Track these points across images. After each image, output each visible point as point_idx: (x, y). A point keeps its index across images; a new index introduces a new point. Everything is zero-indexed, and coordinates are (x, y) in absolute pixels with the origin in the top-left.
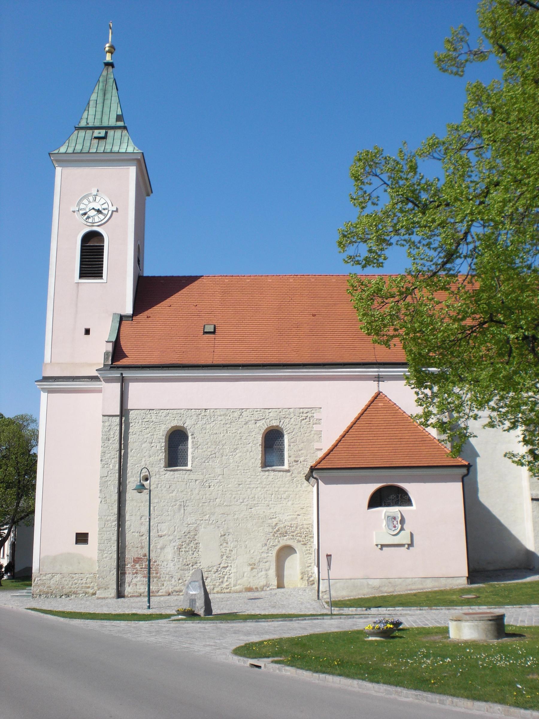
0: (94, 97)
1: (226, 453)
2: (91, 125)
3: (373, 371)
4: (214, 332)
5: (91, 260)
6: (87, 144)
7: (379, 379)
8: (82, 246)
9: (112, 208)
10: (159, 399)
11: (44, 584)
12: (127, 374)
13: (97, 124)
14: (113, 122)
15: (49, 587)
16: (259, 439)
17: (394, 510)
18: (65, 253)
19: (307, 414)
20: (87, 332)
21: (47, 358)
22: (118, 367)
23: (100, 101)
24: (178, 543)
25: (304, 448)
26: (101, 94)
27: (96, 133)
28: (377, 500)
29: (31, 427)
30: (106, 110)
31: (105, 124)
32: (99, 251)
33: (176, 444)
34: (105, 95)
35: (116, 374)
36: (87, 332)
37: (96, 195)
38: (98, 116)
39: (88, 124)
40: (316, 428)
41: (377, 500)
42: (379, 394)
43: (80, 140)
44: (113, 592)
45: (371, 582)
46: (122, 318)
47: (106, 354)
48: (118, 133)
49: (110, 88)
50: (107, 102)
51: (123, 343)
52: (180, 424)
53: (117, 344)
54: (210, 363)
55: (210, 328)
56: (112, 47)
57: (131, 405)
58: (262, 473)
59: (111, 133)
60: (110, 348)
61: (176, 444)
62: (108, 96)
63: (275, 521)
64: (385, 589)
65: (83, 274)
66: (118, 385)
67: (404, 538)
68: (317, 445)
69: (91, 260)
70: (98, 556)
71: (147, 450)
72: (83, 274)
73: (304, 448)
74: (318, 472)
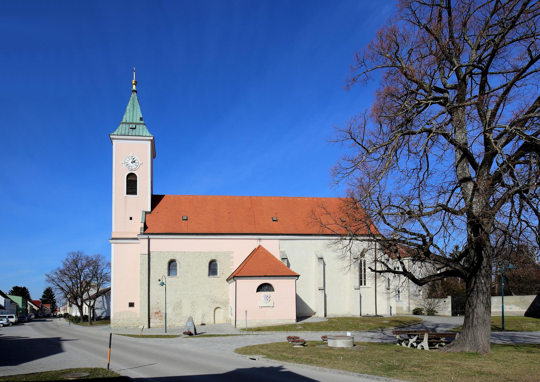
0: (128, 107)
1: (193, 269)
2: (128, 122)
4: (187, 220)
6: (127, 131)
8: (127, 180)
9: (140, 163)
10: (165, 247)
11: (116, 324)
12: (150, 237)
13: (131, 121)
14: (138, 121)
16: (207, 265)
17: (268, 293)
19: (228, 255)
20: (131, 219)
21: (113, 230)
22: (146, 234)
23: (131, 110)
24: (174, 306)
25: (226, 268)
26: (132, 106)
27: (131, 126)
28: (260, 288)
30: (135, 114)
31: (135, 122)
32: (136, 181)
33: (172, 265)
35: (146, 237)
36: (131, 219)
37: (131, 153)
38: (131, 117)
39: (149, 239)
40: (231, 260)
41: (260, 288)
42: (260, 246)
43: (124, 129)
44: (146, 326)
46: (146, 213)
47: (141, 228)
48: (141, 126)
49: (136, 104)
50: (135, 111)
51: (147, 223)
52: (174, 258)
53: (145, 224)
54: (186, 232)
55: (185, 218)
56: (136, 82)
59: (138, 126)
60: (142, 225)
61: (172, 265)
62: (135, 107)
63: (213, 297)
66: (147, 240)
67: (270, 304)
68: (231, 267)
70: (140, 310)
71: (160, 269)
73: (226, 268)
74: (234, 277)
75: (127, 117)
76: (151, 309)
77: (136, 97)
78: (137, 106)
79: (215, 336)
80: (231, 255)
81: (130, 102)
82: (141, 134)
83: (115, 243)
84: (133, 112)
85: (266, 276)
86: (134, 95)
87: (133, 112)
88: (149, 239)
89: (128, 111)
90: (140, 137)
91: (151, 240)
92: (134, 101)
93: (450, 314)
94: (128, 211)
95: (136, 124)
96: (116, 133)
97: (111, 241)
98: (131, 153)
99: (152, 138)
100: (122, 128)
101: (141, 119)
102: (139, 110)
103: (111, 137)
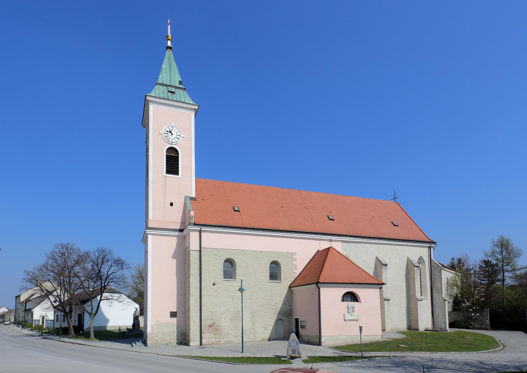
0: (164, 66)
3: (328, 237)
5: (172, 164)
7: (330, 241)
10: (219, 243)
12: (203, 229)
15: (156, 340)
18: (187, 161)
19: (291, 256)
20: (172, 204)
23: (168, 70)
27: (170, 89)
29: (506, 302)
30: (172, 76)
32: (177, 159)
34: (170, 66)
36: (172, 204)
37: (172, 123)
39: (200, 231)
45: (343, 337)
48: (182, 91)
49: (172, 63)
50: (172, 72)
57: (202, 246)
58: (269, 284)
62: (172, 68)
64: (349, 341)
65: (168, 172)
69: (172, 164)
72: (168, 172)
75: (163, 78)
76: (202, 321)
77: (173, 56)
78: (175, 67)
79: (184, 357)
80: (294, 257)
81: (166, 61)
82: (183, 101)
83: (153, 234)
84: (170, 72)
85: (369, 284)
86: (169, 53)
87: (170, 72)
88: (200, 231)
89: (164, 70)
90: (180, 104)
91: (202, 233)
92: (169, 59)
93: (287, 342)
94: (168, 196)
95: (176, 87)
96: (152, 94)
97: (148, 231)
98: (172, 123)
99: (196, 107)
100: (158, 91)
101: (180, 83)
102: (177, 71)
103: (148, 98)
